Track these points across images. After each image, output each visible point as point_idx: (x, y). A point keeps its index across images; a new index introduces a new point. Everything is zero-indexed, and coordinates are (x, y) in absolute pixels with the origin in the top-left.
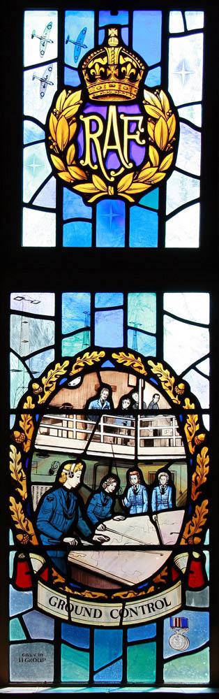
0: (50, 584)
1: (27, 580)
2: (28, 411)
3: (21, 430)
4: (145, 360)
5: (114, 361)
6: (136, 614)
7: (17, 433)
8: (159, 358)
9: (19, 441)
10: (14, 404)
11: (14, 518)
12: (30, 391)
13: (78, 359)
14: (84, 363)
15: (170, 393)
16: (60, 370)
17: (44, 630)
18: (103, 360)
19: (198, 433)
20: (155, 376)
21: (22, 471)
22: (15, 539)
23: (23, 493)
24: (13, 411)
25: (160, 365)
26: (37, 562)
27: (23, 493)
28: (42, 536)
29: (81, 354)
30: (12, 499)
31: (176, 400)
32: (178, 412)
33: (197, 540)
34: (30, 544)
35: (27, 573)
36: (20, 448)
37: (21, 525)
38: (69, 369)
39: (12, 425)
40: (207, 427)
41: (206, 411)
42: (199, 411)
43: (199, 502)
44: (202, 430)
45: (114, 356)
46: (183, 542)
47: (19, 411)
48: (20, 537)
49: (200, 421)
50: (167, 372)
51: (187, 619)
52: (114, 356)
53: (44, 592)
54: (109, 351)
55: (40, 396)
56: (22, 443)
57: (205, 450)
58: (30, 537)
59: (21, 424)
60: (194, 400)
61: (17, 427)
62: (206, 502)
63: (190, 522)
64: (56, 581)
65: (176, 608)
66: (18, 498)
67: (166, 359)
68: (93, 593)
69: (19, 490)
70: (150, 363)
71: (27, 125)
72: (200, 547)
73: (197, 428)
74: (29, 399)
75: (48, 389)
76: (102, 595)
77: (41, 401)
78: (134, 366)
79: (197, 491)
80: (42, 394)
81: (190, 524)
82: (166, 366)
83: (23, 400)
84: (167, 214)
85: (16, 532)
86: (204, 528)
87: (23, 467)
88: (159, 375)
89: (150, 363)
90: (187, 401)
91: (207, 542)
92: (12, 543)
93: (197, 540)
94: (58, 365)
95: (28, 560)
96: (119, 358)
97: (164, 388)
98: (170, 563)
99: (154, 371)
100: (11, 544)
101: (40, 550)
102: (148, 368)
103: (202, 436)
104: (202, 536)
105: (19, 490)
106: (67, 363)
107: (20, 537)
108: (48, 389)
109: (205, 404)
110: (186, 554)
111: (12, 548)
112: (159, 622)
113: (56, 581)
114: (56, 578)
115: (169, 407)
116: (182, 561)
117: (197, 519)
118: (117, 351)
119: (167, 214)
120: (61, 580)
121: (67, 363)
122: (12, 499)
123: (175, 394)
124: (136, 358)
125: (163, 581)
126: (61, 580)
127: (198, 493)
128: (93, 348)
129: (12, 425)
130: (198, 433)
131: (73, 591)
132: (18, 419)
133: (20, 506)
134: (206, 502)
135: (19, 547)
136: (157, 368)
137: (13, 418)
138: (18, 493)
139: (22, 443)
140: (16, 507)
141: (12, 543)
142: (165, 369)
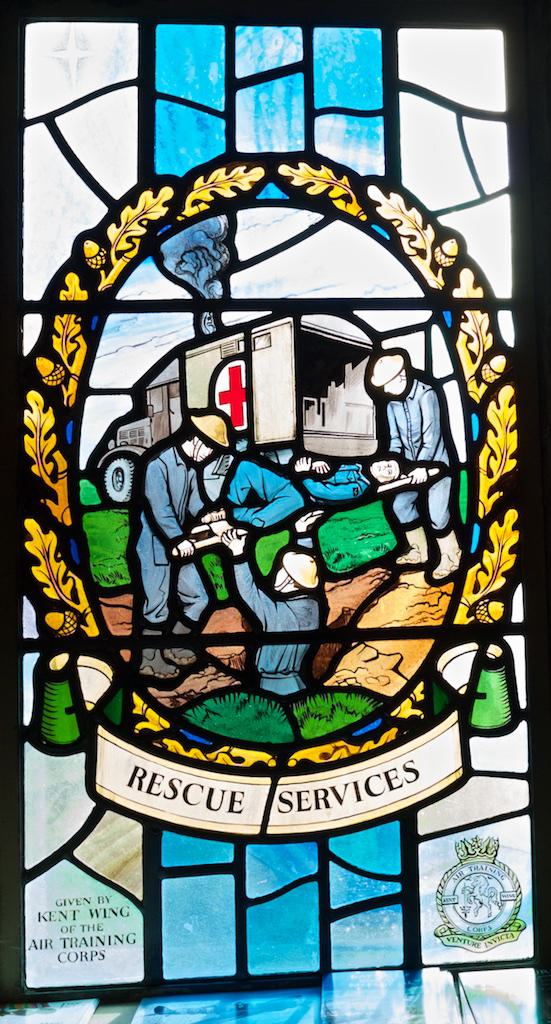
0: (125, 730)
1: (65, 729)
2: (71, 307)
3: (55, 357)
4: (359, 183)
5: (284, 183)
6: (340, 801)
7: (44, 365)
8: (391, 181)
9: (50, 382)
10: (34, 288)
11: (39, 573)
12: (77, 262)
13: (199, 182)
14: (212, 193)
15: (423, 266)
16: (154, 205)
17: (118, 842)
18: (258, 186)
19: (488, 356)
20: (388, 225)
21: (70, 574)
22: (41, 624)
23: (60, 510)
24: (33, 307)
25: (396, 199)
26: (95, 678)
27: (60, 510)
28: (176, 363)
29: (205, 170)
30: (31, 525)
31: (436, 282)
32: (443, 308)
33: (496, 609)
34: (80, 633)
35: (69, 711)
36: (52, 397)
37: (58, 590)
38: (176, 205)
39: (29, 342)
40: (509, 336)
41: (504, 305)
42: (489, 305)
43: (497, 514)
44: (498, 347)
45: (284, 170)
46: (461, 618)
47: (50, 305)
48: (54, 620)
49: (494, 328)
50: (414, 213)
51: (66, 709)
52: (284, 170)
53: (116, 756)
54: (269, 161)
55: (102, 272)
56: (78, 629)
57: (507, 393)
58: (81, 619)
59: (57, 344)
60: (480, 280)
61: (44, 347)
62: (511, 516)
63: (478, 566)
64: (140, 726)
65: (453, 779)
66: (48, 523)
67: (407, 182)
68: (236, 752)
69: (49, 503)
70: (374, 192)
71: (87, 704)
72: (505, 626)
73: (489, 342)
74: (72, 280)
75: (120, 254)
76: (264, 757)
77: (105, 282)
78: (332, 194)
79: (490, 494)
80: (108, 267)
81: (479, 570)
82: (411, 201)
83: (57, 283)
84: (29, 865)
85: (43, 606)
86: (512, 577)
87: (70, 566)
88: (395, 223)
89: (374, 192)
90: (466, 276)
91: (518, 616)
92: (30, 631)
93: (496, 609)
94: (146, 196)
95: (70, 674)
96: (301, 175)
97: (408, 250)
98: (429, 672)
99: (384, 212)
100: (26, 635)
101: (104, 647)
102: (369, 206)
103: (499, 363)
104: (504, 595)
105: (49, 503)
106: (167, 193)
107: (54, 620)
108: (120, 254)
109: (503, 288)
110: (474, 646)
111: (30, 645)
112: (407, 818)
113: (140, 726)
114: (143, 718)
115: (421, 294)
116: (457, 667)
117: (494, 556)
118: (292, 159)
119: (29, 865)
120: (155, 722)
121: (167, 193)
122: (31, 525)
123: (435, 267)
124: (339, 177)
125: (418, 712)
126: (155, 722)
127: (496, 496)
128: (231, 158)
129: (29, 342)
130: (488, 356)
131: (187, 749)
132: (48, 331)
133: (52, 539)
134: (511, 516)
135: (49, 642)
136: (390, 207)
137: (32, 325)
138: (48, 510)
139: (78, 629)
140: (39, 541)
141: (30, 631)
142: (409, 208)
